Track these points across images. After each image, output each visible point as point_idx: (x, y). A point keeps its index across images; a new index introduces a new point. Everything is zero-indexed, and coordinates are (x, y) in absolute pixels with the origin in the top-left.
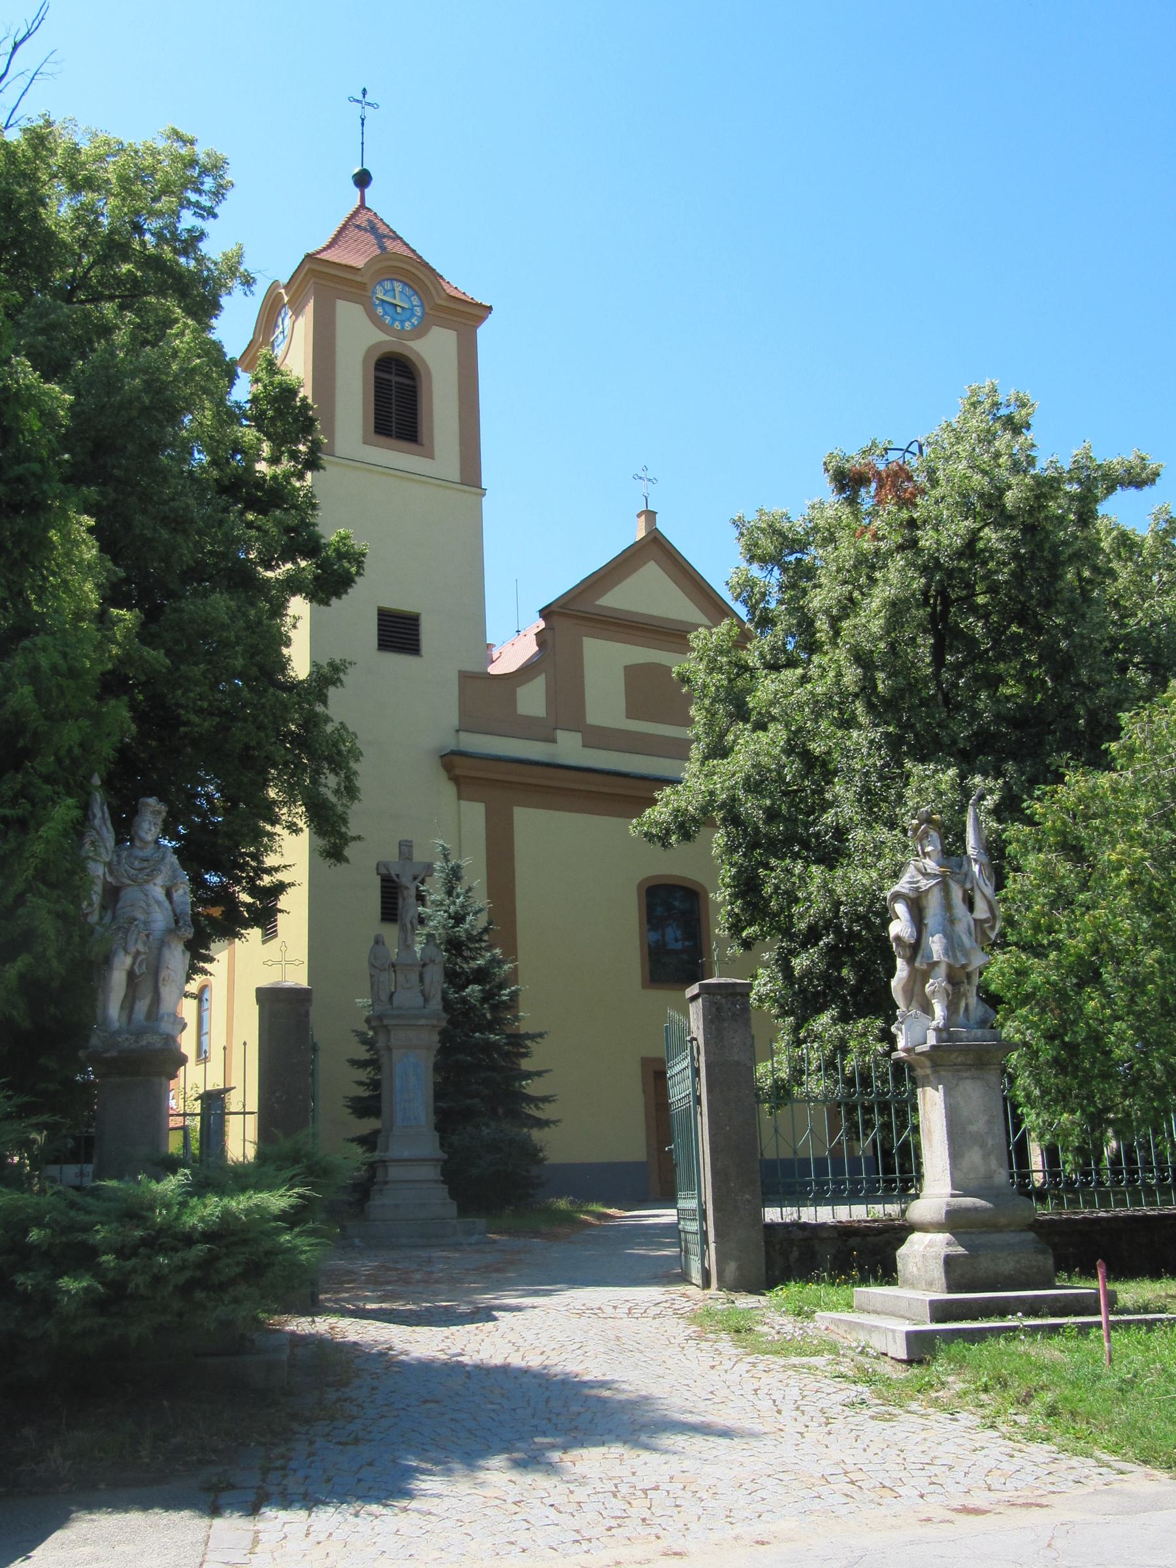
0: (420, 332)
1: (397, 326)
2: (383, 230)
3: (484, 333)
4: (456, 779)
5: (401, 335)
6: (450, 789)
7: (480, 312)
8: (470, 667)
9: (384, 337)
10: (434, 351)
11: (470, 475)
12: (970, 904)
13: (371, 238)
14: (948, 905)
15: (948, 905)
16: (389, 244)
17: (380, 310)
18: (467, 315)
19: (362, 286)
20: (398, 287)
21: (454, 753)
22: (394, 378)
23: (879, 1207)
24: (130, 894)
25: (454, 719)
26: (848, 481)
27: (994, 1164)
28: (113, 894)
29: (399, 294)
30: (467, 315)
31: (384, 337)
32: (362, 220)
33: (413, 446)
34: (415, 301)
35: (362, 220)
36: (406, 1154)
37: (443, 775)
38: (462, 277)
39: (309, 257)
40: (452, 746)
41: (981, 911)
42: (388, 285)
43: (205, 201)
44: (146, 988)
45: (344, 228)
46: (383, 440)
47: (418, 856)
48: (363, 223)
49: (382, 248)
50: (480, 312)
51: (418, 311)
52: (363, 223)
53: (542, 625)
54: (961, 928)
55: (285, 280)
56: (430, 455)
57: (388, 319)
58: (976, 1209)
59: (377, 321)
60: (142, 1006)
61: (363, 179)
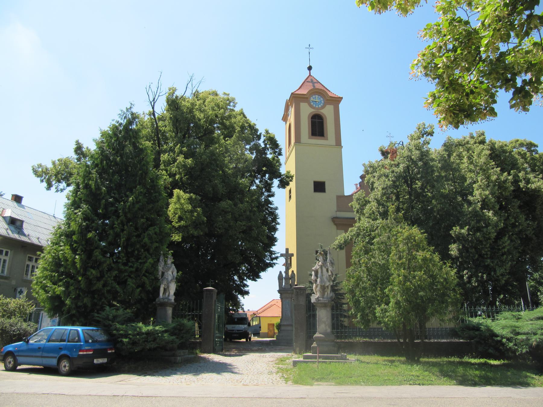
0: (323, 107)
1: (317, 106)
2: (315, 81)
3: (341, 105)
4: (336, 224)
5: (319, 109)
6: (334, 227)
7: (339, 99)
8: (339, 194)
9: (312, 110)
10: (327, 112)
11: (338, 143)
12: (327, 271)
13: (311, 84)
14: (322, 272)
15: (322, 272)
16: (316, 85)
17: (312, 103)
18: (336, 101)
19: (307, 98)
20: (317, 96)
21: (334, 218)
22: (317, 120)
23: (196, 332)
24: (166, 273)
25: (335, 209)
26: (384, 153)
27: (327, 328)
28: (163, 273)
29: (316, 98)
30: (336, 101)
31: (312, 110)
32: (309, 80)
33: (322, 138)
34: (322, 99)
35: (309, 80)
36: (285, 323)
37: (332, 223)
38: (335, 90)
39: (292, 93)
40: (335, 216)
41: (330, 273)
42: (314, 96)
43: (231, 108)
44: (167, 290)
45: (304, 82)
46: (314, 137)
47: (290, 252)
48: (310, 80)
49: (314, 86)
50: (339, 99)
51: (323, 102)
52: (310, 80)
53: (361, 180)
54: (324, 277)
55: (288, 99)
56: (327, 139)
57: (314, 105)
58: (321, 337)
59: (311, 106)
60: (167, 294)
61: (310, 68)
